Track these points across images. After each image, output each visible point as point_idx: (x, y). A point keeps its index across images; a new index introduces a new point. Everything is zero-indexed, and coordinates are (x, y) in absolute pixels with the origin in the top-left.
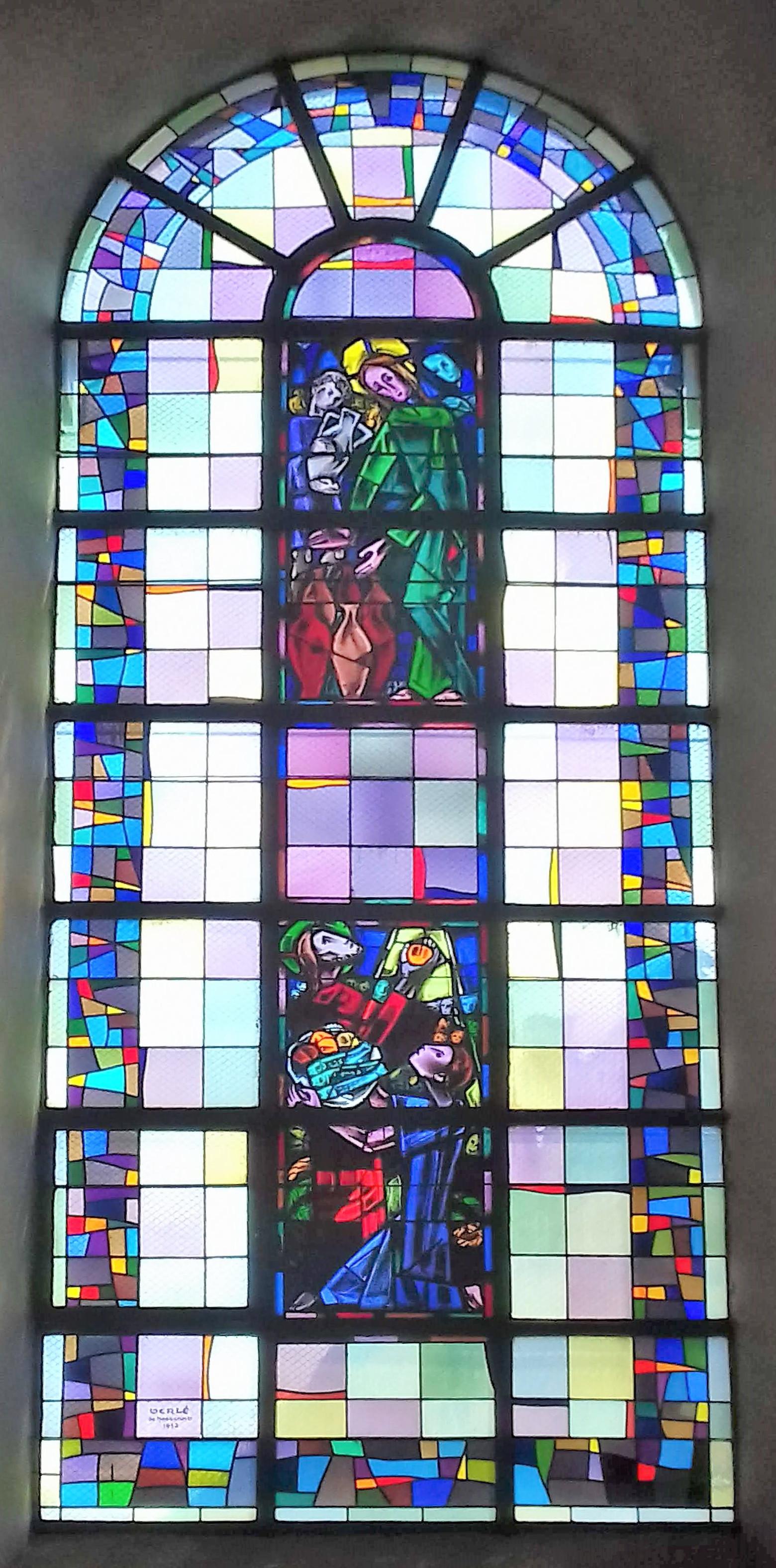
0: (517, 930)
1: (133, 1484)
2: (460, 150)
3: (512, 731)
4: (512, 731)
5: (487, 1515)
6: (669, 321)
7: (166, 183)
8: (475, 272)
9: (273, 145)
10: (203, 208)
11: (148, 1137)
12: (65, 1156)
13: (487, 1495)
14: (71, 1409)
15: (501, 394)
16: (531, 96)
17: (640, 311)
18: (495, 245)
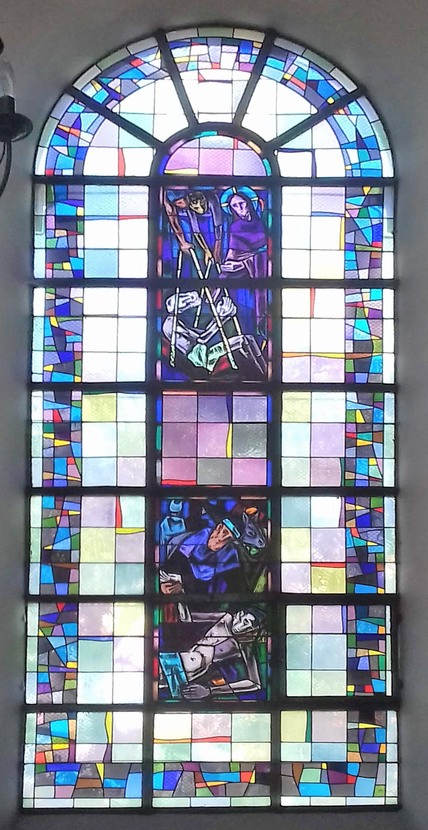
0: (287, 294)
1: (74, 787)
7: (94, 98)
10: (115, 113)
12: (43, 342)
18: (278, 135)
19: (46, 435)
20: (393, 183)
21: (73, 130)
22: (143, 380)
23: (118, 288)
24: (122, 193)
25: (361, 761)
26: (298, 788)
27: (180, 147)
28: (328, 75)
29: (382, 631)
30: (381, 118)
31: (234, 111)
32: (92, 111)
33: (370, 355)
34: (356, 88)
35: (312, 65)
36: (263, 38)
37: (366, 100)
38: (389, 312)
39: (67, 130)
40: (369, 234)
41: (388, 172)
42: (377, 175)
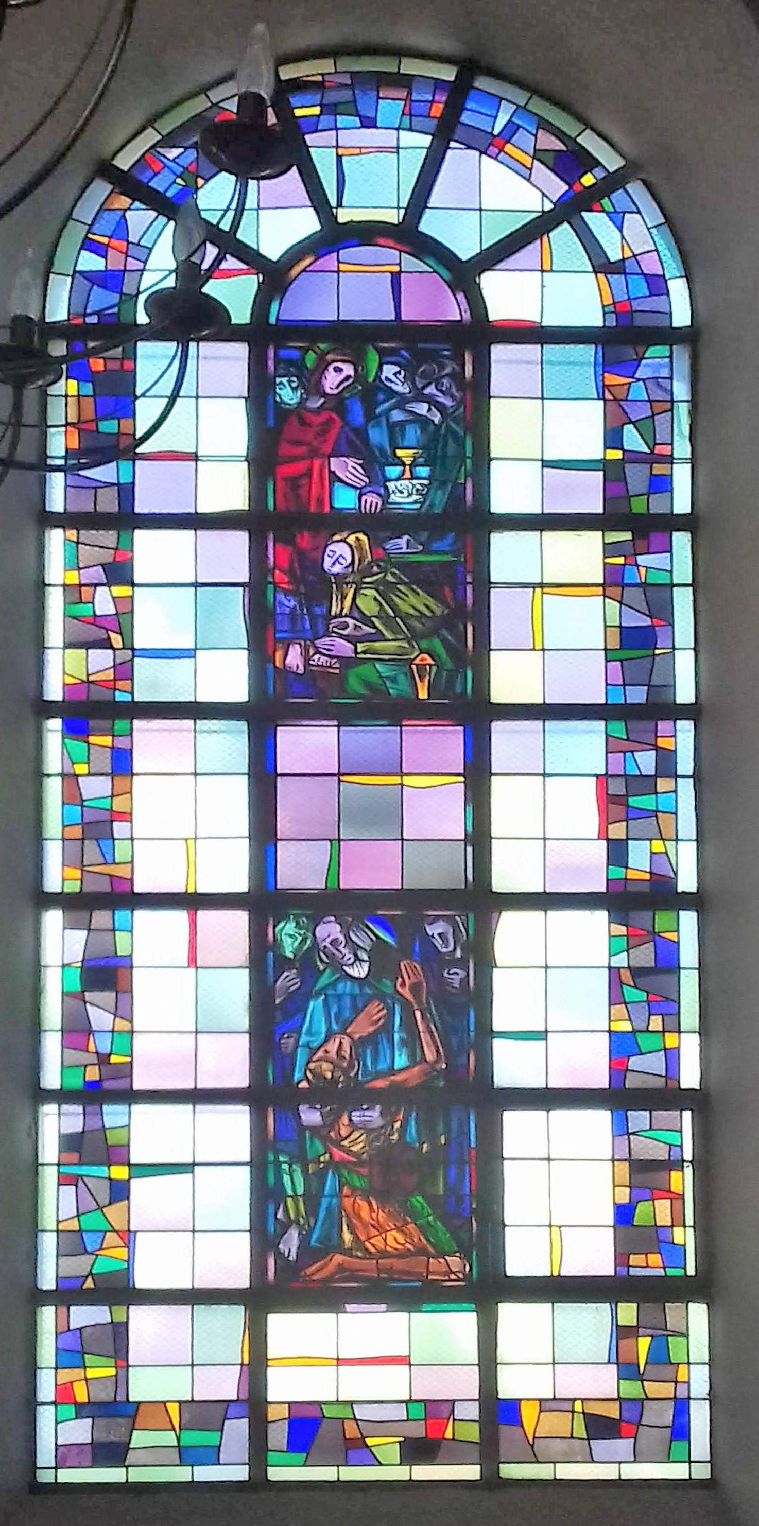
2: (449, 153)
3: (499, 728)
4: (499, 728)
5: (471, 1472)
8: (463, 275)
11: (600, 699)
13: (475, 1453)
15: (490, 397)
16: (521, 97)
21: (114, 243)
22: (245, 698)
27: (304, 270)
31: (404, 204)
32: (144, 207)
33: (650, 652)
39: (105, 240)
42: (663, 322)
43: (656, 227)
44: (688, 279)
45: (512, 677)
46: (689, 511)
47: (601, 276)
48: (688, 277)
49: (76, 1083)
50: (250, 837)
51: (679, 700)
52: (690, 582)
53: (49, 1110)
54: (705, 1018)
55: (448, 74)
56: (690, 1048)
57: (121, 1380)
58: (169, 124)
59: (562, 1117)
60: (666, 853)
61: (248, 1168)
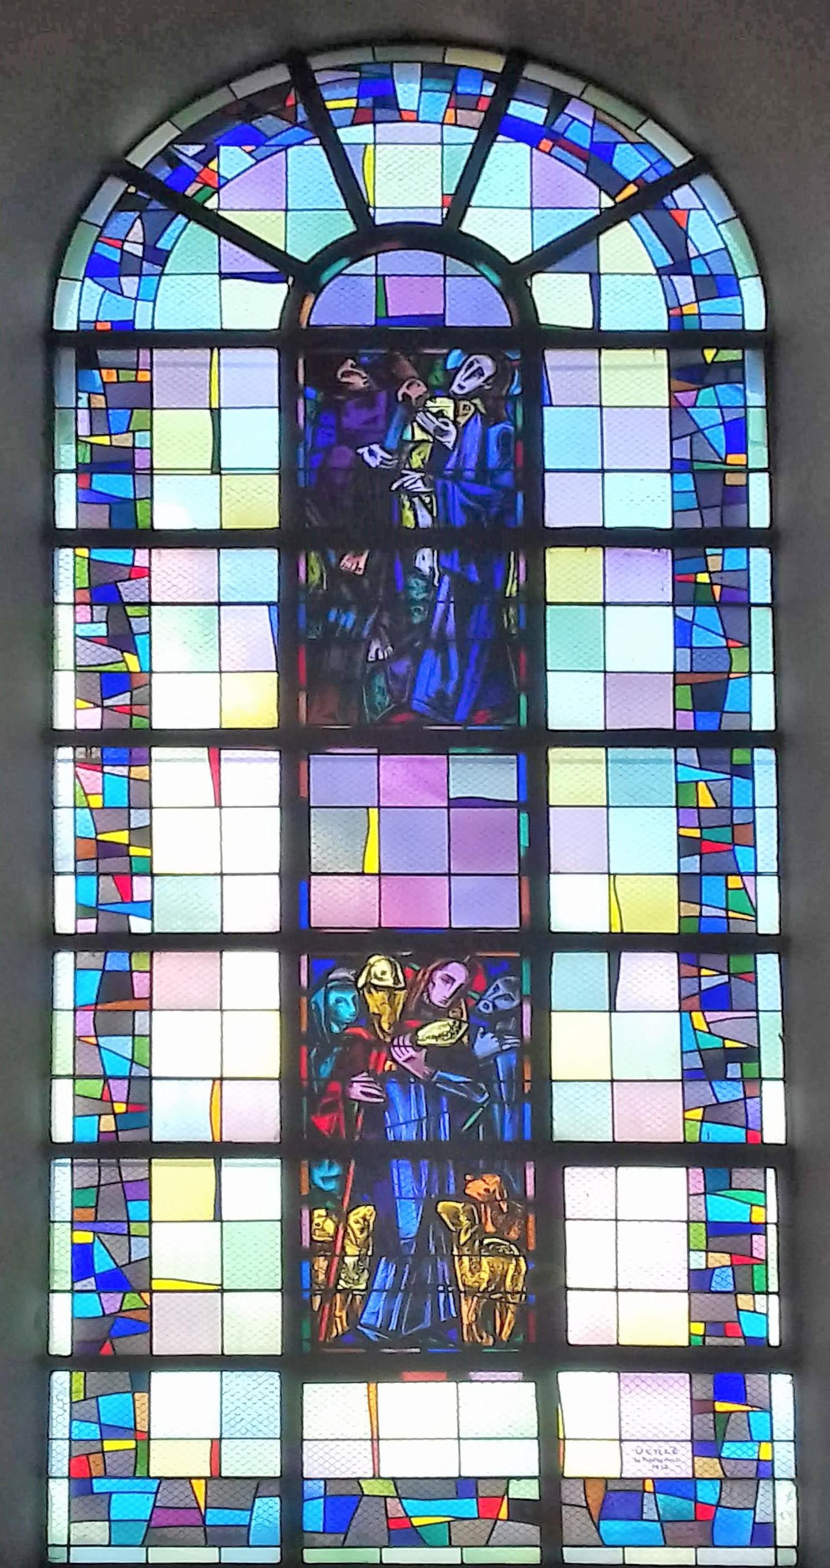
6: (734, 324)
8: (514, 279)
9: (286, 143)
14: (79, 1449)
17: (700, 314)
19: (147, 852)
20: (766, 342)
23: (221, 529)
24: (225, 365)
25: (723, 1476)
26: (598, 1529)
28: (633, 133)
29: (758, 1216)
30: (741, 215)
34: (690, 157)
35: (599, 114)
36: (502, 65)
37: (712, 180)
38: (760, 591)
40: (718, 438)
41: (755, 320)
43: (725, 222)
44: (762, 280)
45: (572, 701)
46: (772, 727)
47: (665, 278)
48: (763, 275)
49: (89, 1134)
50: (280, 806)
51: (767, 1139)
52: (766, 466)
53: (65, 557)
54: (789, 1054)
55: (496, 64)
56: (767, 894)
57: (142, 1454)
58: (189, 117)
59: (632, 1176)
60: (745, 888)
61: (277, 1083)
